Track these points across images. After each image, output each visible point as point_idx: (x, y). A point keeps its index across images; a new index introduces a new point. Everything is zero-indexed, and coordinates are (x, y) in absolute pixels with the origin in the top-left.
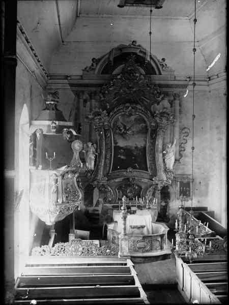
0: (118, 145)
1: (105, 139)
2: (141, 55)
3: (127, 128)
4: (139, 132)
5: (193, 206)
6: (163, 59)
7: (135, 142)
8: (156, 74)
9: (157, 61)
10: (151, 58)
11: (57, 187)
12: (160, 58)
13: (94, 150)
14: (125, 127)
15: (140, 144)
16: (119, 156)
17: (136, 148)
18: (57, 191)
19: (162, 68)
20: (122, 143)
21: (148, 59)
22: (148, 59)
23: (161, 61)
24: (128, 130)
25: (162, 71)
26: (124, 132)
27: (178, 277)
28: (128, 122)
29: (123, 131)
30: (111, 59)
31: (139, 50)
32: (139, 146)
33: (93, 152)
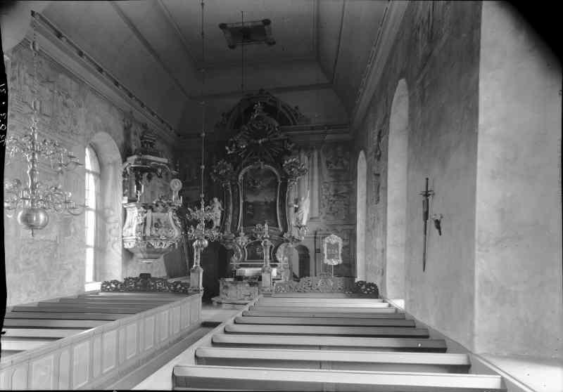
1: (233, 195)
2: (271, 104)
3: (256, 182)
4: (269, 186)
5: (407, 92)
6: (297, 108)
7: (263, 197)
8: (290, 125)
10: (284, 107)
11: (145, 219)
12: (293, 106)
13: (220, 205)
14: (254, 181)
15: (270, 199)
16: (227, 148)
17: (266, 203)
18: (145, 223)
20: (251, 199)
21: (281, 109)
22: (281, 109)
24: (257, 184)
25: (296, 121)
27: (471, 373)
30: (242, 110)
32: (269, 202)
33: (219, 208)
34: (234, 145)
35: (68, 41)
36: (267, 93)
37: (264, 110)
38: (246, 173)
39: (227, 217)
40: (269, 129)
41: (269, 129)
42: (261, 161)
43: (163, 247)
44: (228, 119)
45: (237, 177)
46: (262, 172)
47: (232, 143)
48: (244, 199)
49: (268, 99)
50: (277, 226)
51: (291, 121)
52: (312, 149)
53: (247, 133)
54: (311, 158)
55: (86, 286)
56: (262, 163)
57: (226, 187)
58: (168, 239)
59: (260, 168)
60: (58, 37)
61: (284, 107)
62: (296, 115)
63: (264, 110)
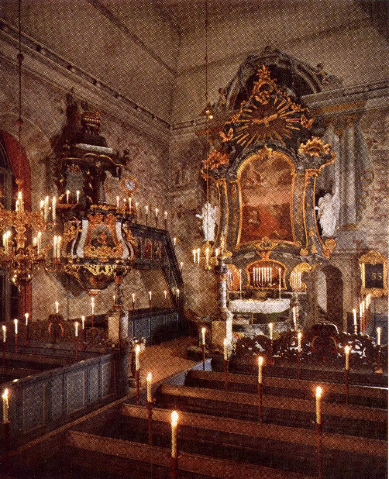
0: (249, 204)
2: (283, 66)
3: (262, 178)
9: (309, 71)
14: (258, 178)
19: (321, 81)
21: (297, 71)
22: (297, 71)
23: (316, 68)
26: (257, 185)
28: (262, 170)
29: (255, 183)
31: (277, 59)
34: (231, 130)
35: (143, 110)
36: (276, 51)
37: (272, 76)
38: (247, 168)
39: (348, 320)
40: (279, 102)
41: (279, 102)
42: (269, 147)
43: (106, 273)
44: (226, 96)
45: (235, 172)
46: (269, 163)
47: (228, 127)
48: (245, 201)
49: (277, 59)
50: (317, 181)
51: (312, 87)
52: (346, 124)
53: (250, 111)
54: (343, 137)
55: (206, 370)
56: (270, 150)
57: (221, 187)
58: (111, 261)
59: (266, 158)
60: (136, 109)
61: (300, 68)
62: (320, 77)
63: (272, 76)
